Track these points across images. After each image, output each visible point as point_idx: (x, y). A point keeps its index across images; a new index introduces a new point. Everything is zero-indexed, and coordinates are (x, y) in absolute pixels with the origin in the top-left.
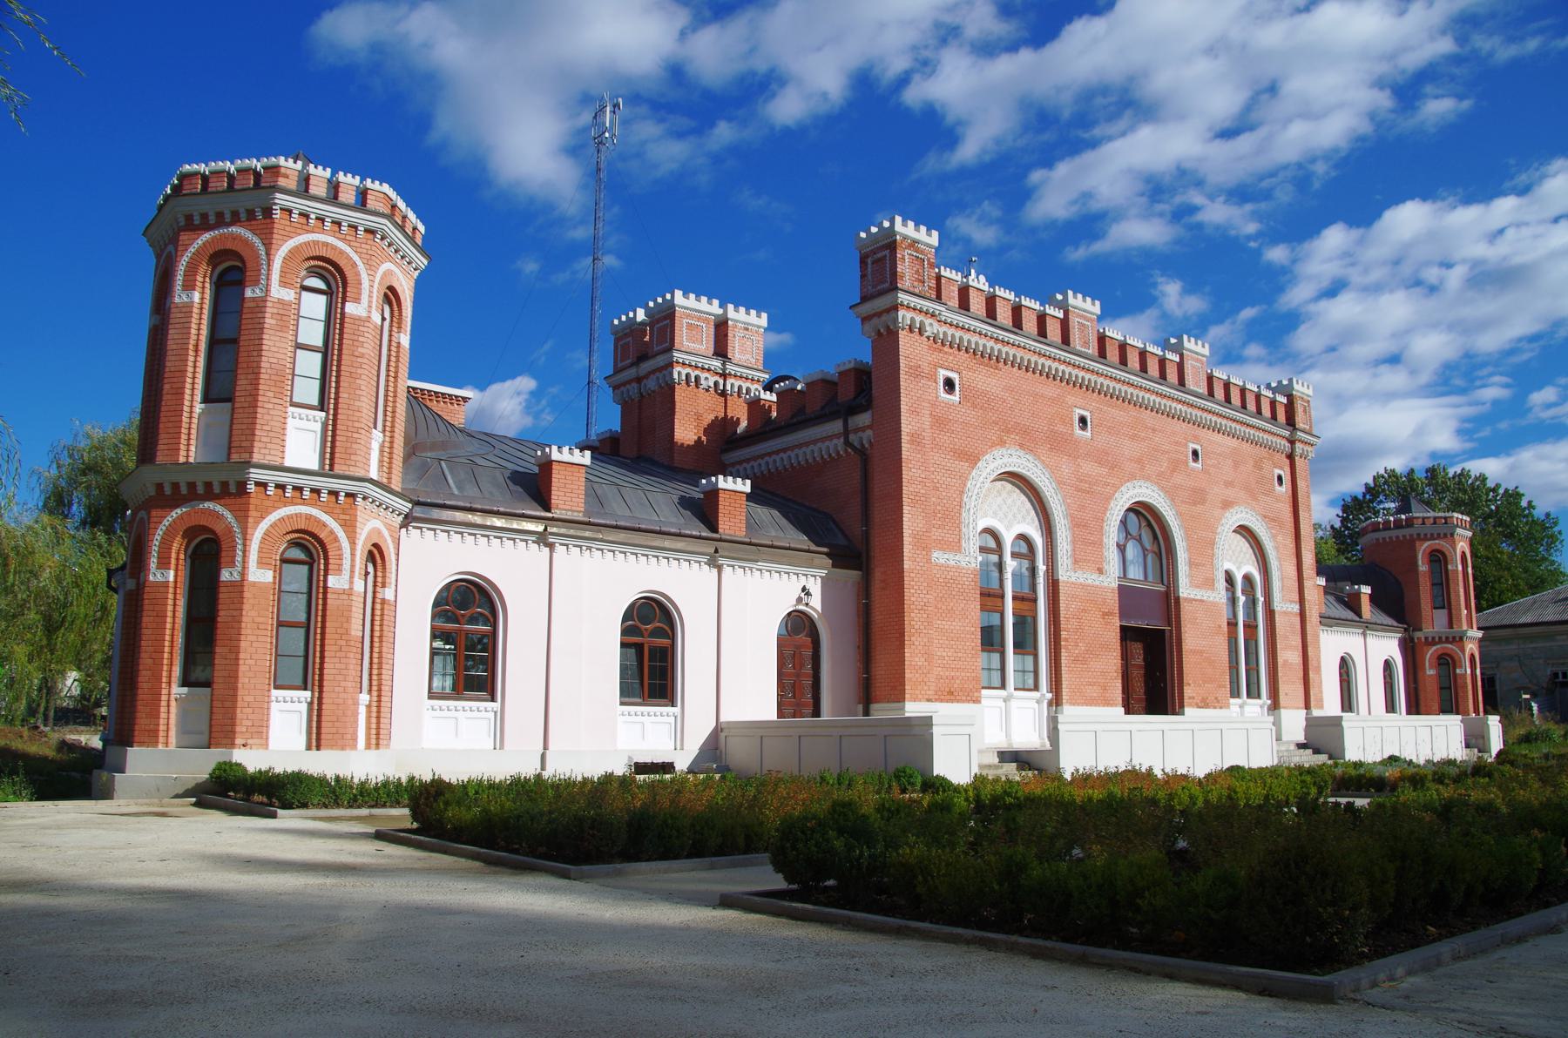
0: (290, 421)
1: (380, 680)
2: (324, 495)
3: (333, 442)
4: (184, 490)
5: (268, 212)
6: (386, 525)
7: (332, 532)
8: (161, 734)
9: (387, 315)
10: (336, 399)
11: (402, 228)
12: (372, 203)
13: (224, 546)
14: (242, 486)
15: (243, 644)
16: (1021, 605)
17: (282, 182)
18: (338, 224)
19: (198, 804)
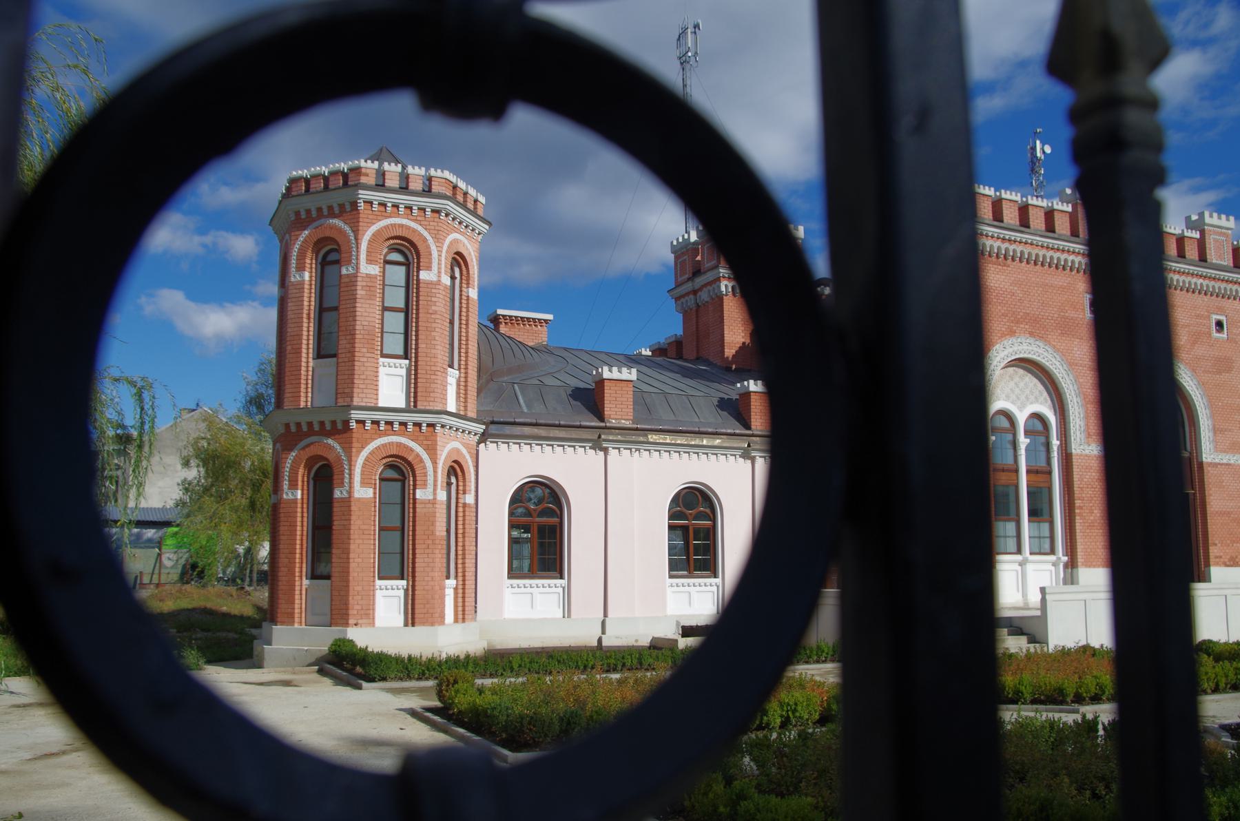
0: (381, 369)
1: (464, 568)
2: (410, 427)
3: (416, 383)
4: (305, 428)
5: (354, 205)
6: (464, 445)
7: (418, 455)
8: (297, 615)
9: (457, 274)
10: (416, 349)
11: (464, 206)
12: (436, 188)
13: (336, 471)
14: (346, 423)
15: (352, 547)
16: (1033, 477)
17: (363, 180)
18: (410, 208)
19: (321, 672)
